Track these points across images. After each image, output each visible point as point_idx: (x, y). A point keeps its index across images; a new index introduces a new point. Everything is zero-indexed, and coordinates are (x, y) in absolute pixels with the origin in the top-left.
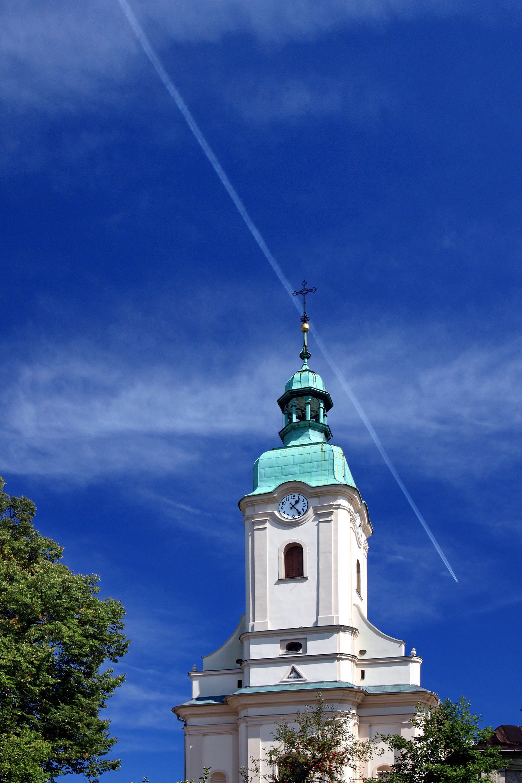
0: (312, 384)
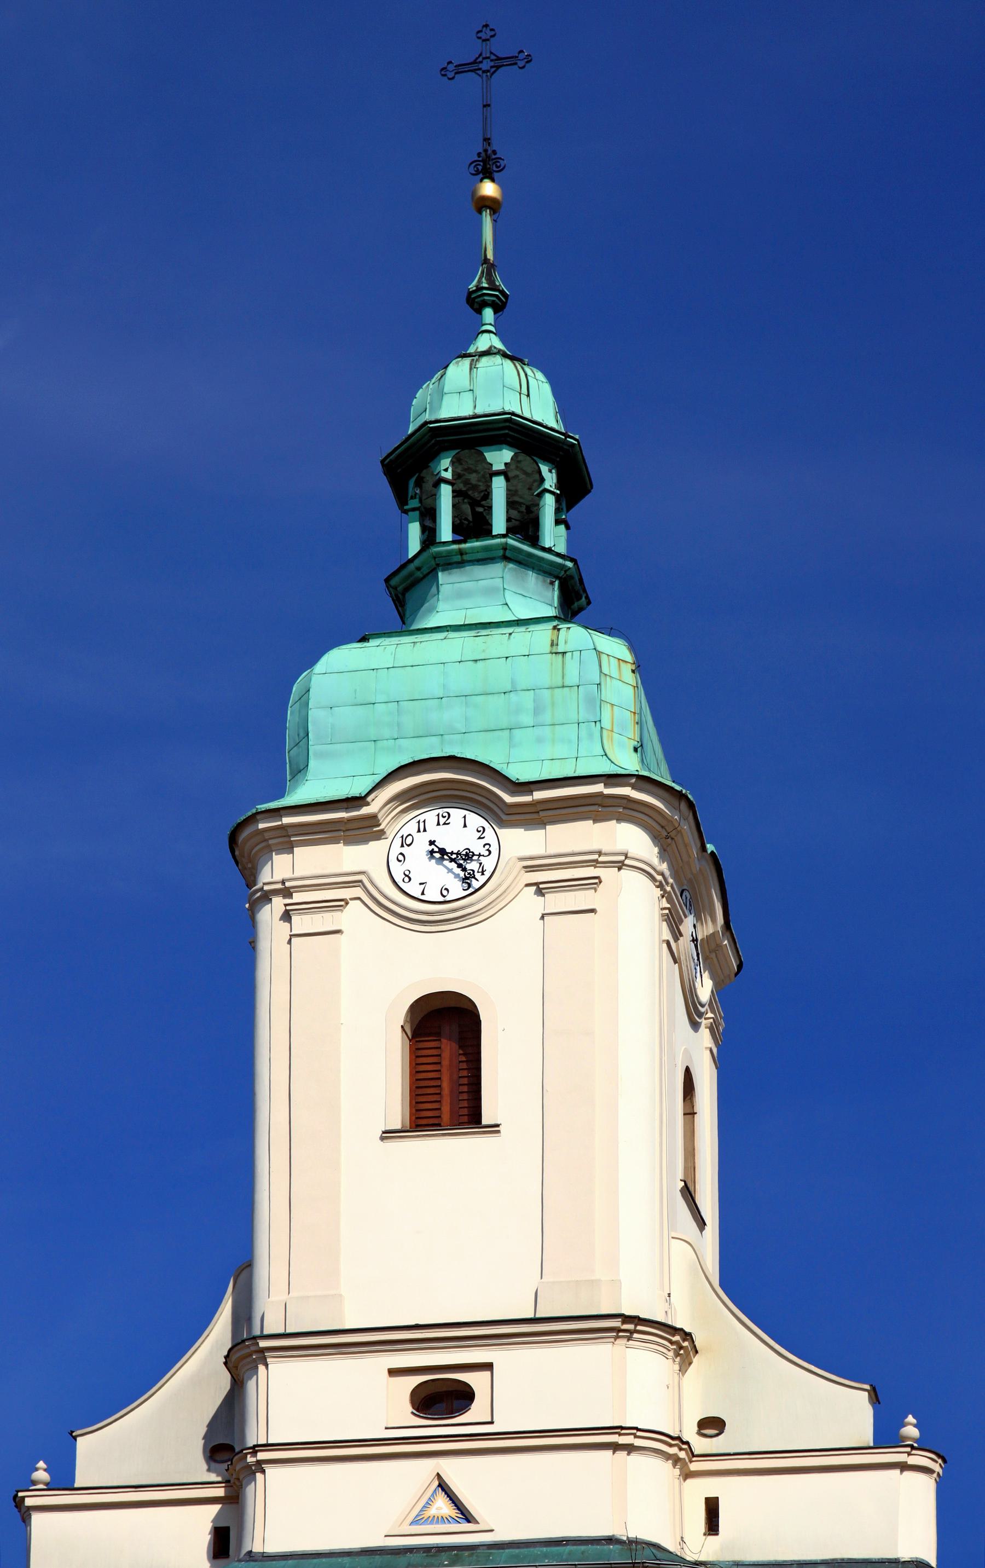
0: (512, 404)
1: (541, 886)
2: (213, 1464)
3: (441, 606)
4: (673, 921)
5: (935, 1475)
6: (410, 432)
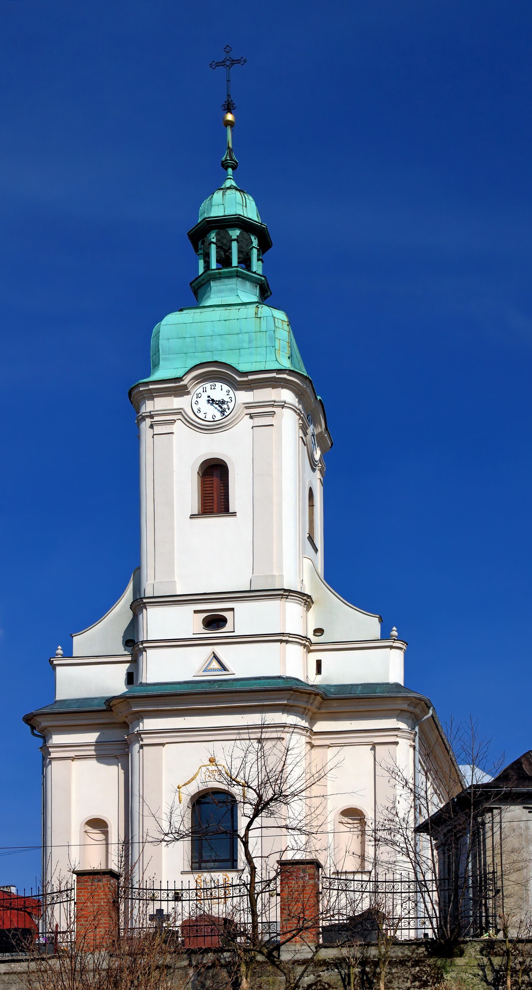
0: (239, 211)
2: (127, 648)
3: (212, 296)
4: (304, 428)
5: (403, 650)
6: (199, 221)
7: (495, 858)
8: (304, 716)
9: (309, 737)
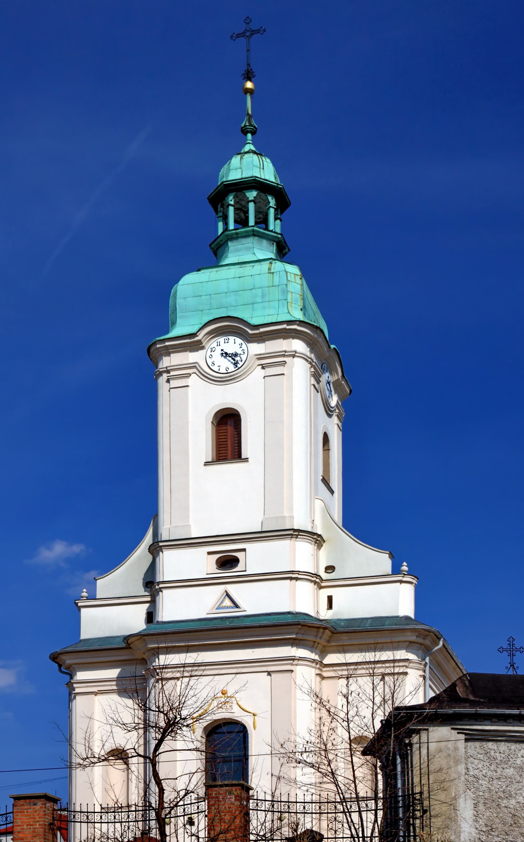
0: (256, 173)
1: (264, 365)
2: (147, 589)
3: (229, 255)
4: (316, 376)
5: (414, 584)
7: (423, 778)
8: (314, 649)
9: (319, 669)
